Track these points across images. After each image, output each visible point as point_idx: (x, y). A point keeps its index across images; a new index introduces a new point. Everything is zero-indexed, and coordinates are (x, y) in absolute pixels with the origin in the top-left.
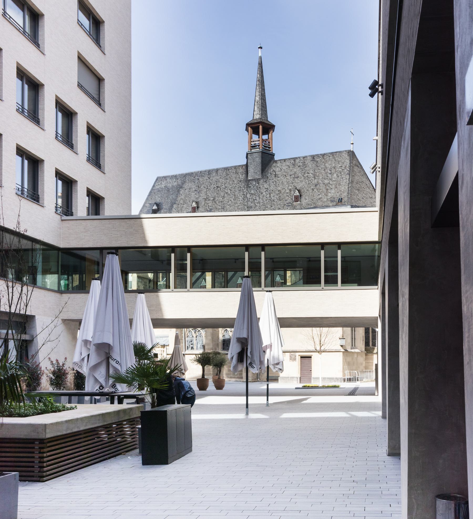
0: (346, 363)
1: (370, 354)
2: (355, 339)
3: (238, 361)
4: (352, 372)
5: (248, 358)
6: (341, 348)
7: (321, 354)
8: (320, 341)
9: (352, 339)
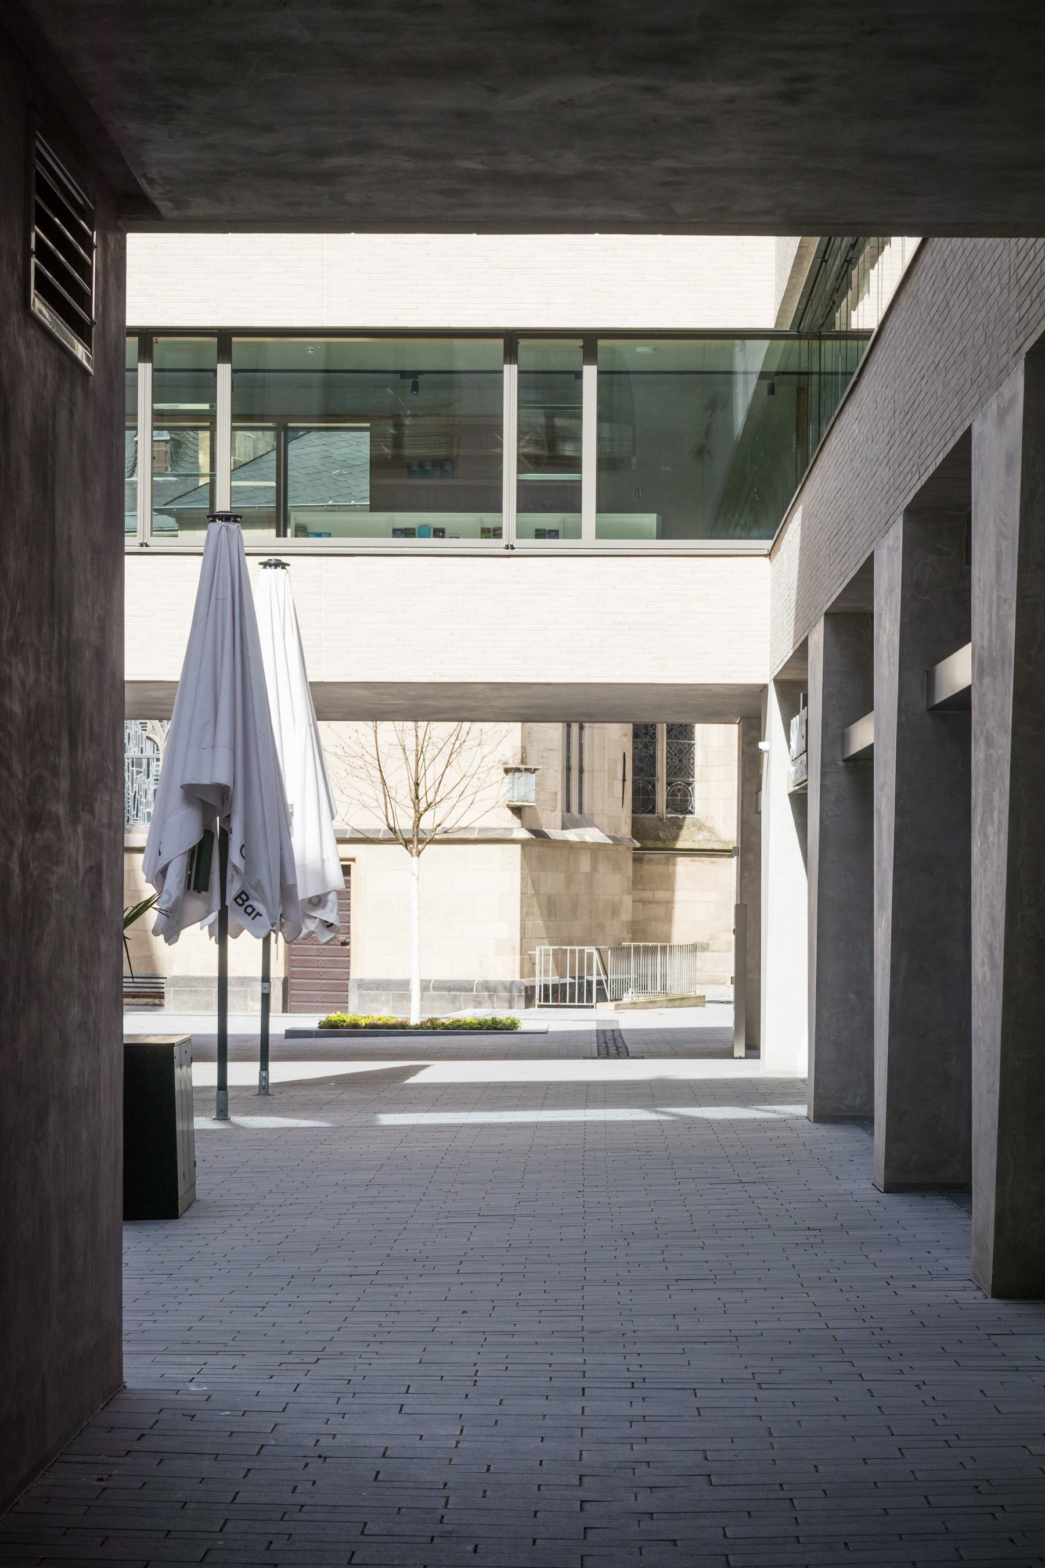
0: (539, 903)
1: (658, 856)
2: (581, 771)
3: (189, 888)
4: (573, 952)
5: (230, 870)
6: (516, 822)
7: (419, 853)
8: (417, 784)
9: (568, 769)
